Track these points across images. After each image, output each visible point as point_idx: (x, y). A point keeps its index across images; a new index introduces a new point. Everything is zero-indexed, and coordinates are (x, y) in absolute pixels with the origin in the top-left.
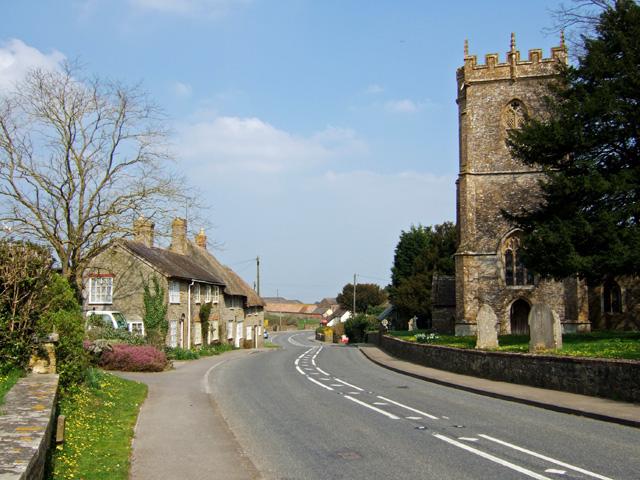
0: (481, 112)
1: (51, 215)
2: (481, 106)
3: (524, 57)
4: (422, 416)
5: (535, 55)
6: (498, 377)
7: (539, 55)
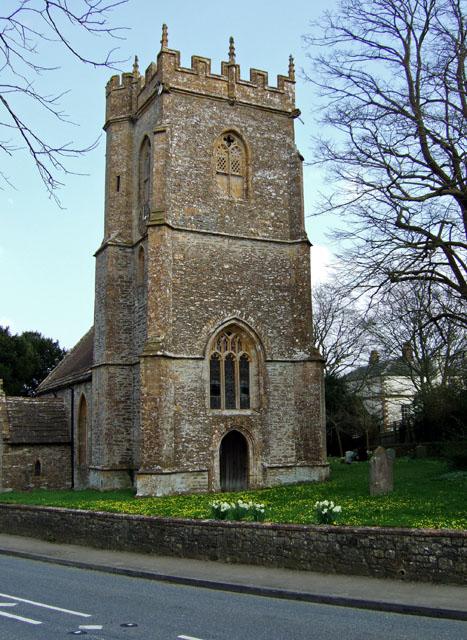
0: (185, 137)
1: (429, 141)
2: (185, 128)
3: (245, 76)
4: (17, 601)
5: (258, 77)
6: (164, 550)
7: (208, 67)
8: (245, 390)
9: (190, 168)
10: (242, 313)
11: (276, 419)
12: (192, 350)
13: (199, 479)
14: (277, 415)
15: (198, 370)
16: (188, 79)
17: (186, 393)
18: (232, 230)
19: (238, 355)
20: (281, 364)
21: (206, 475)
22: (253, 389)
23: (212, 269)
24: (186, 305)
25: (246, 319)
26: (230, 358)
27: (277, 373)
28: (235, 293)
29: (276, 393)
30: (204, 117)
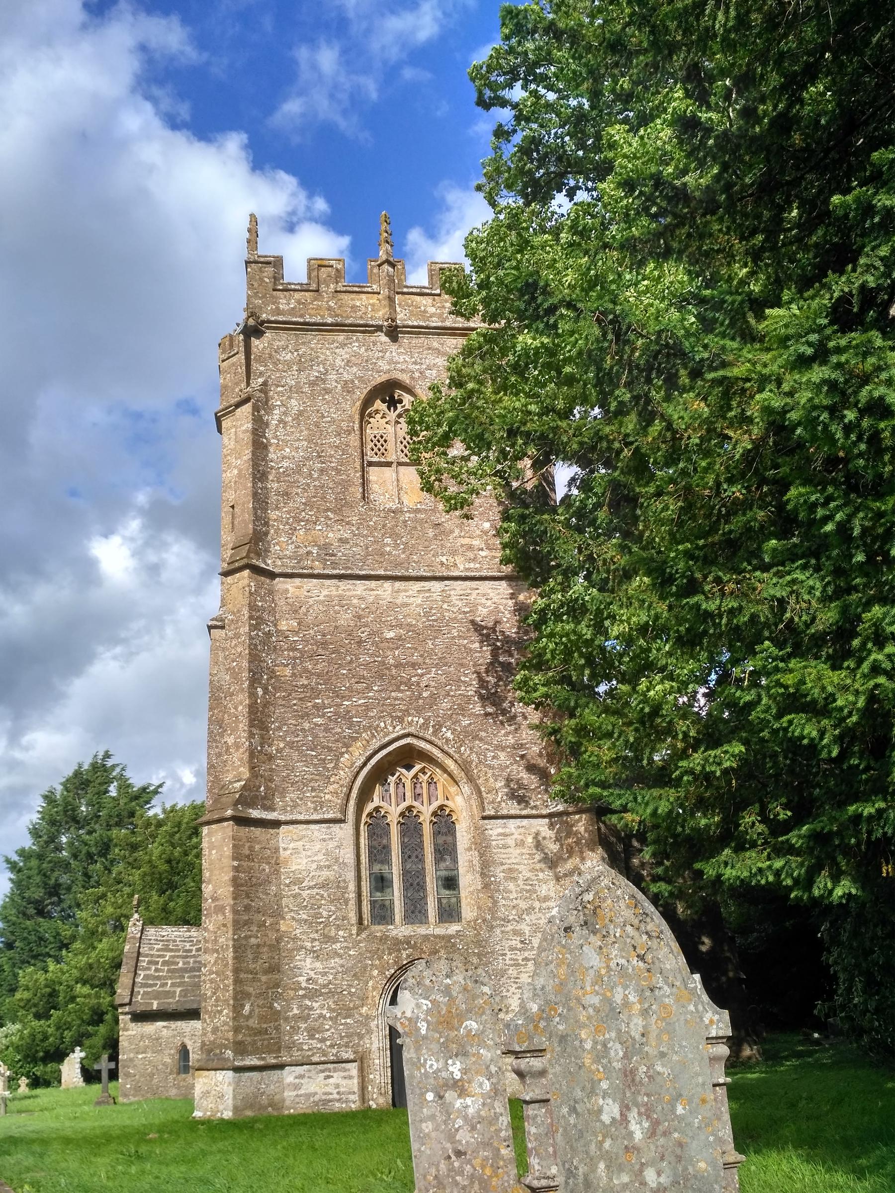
2: (298, 389)
8: (450, 883)
9: (307, 459)
10: (427, 720)
11: (516, 942)
12: (320, 805)
13: (337, 1078)
14: (516, 933)
15: (331, 845)
16: (299, 302)
17: (305, 894)
18: (397, 565)
19: (426, 812)
20: (518, 822)
21: (353, 1069)
22: (468, 881)
23: (360, 642)
24: (306, 716)
25: (435, 733)
26: (409, 818)
27: (510, 841)
28: (409, 684)
29: (511, 886)
30: (333, 366)
